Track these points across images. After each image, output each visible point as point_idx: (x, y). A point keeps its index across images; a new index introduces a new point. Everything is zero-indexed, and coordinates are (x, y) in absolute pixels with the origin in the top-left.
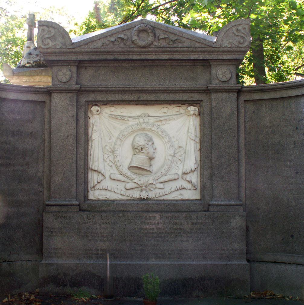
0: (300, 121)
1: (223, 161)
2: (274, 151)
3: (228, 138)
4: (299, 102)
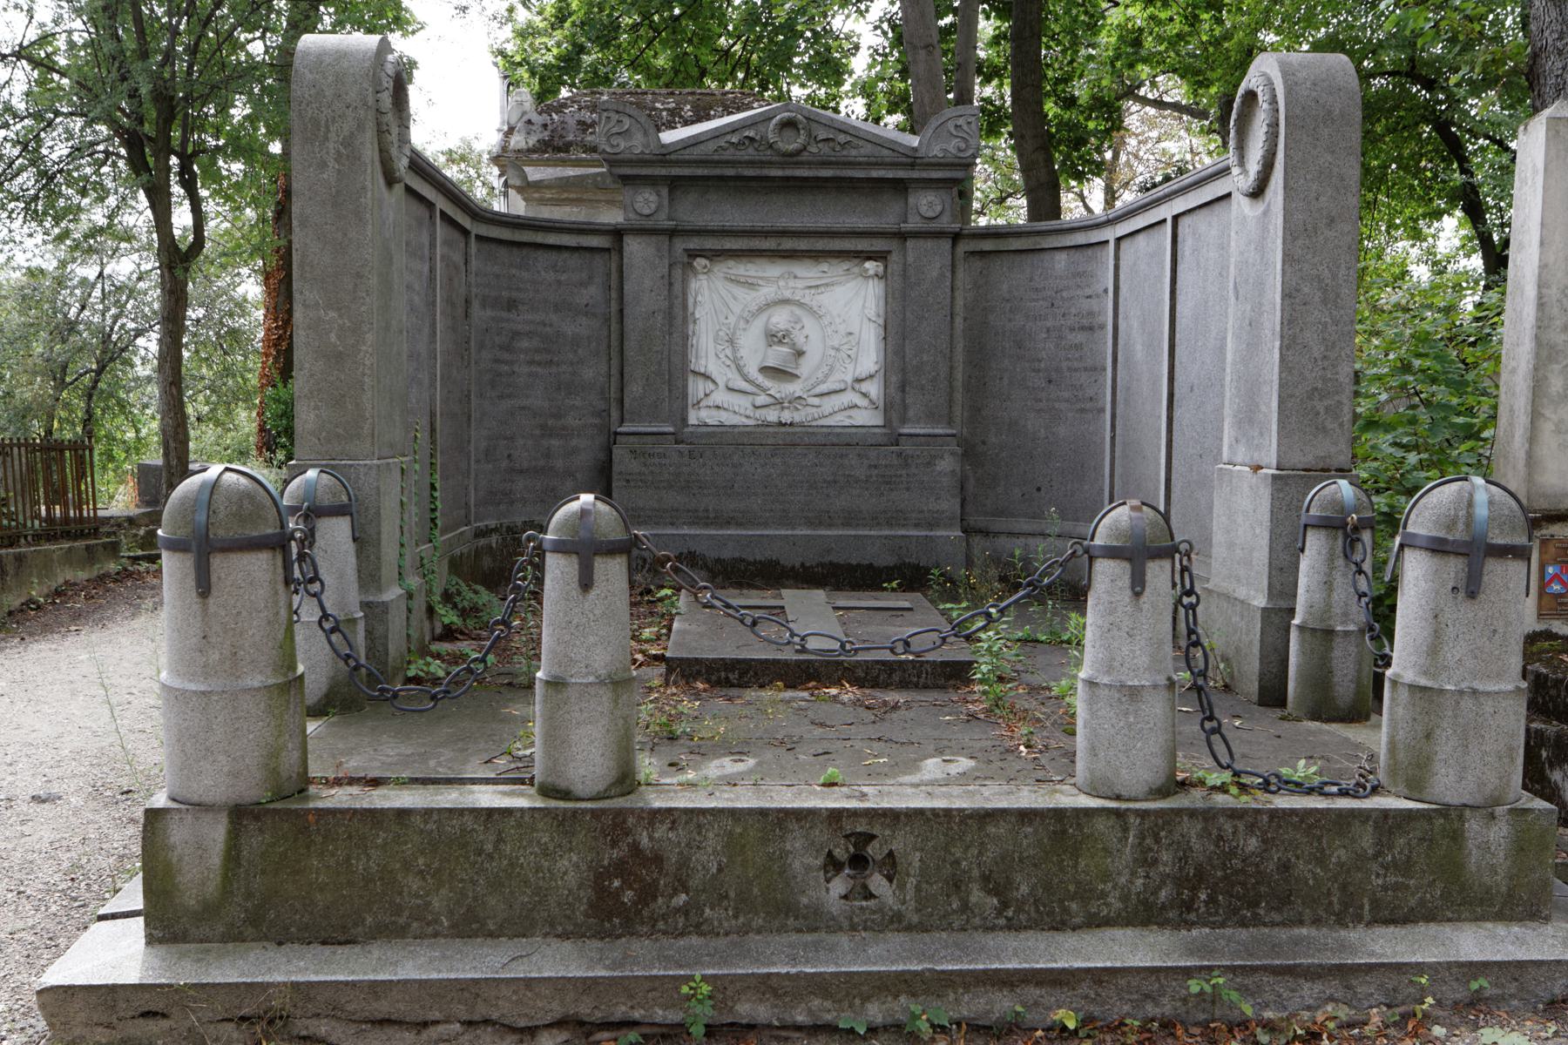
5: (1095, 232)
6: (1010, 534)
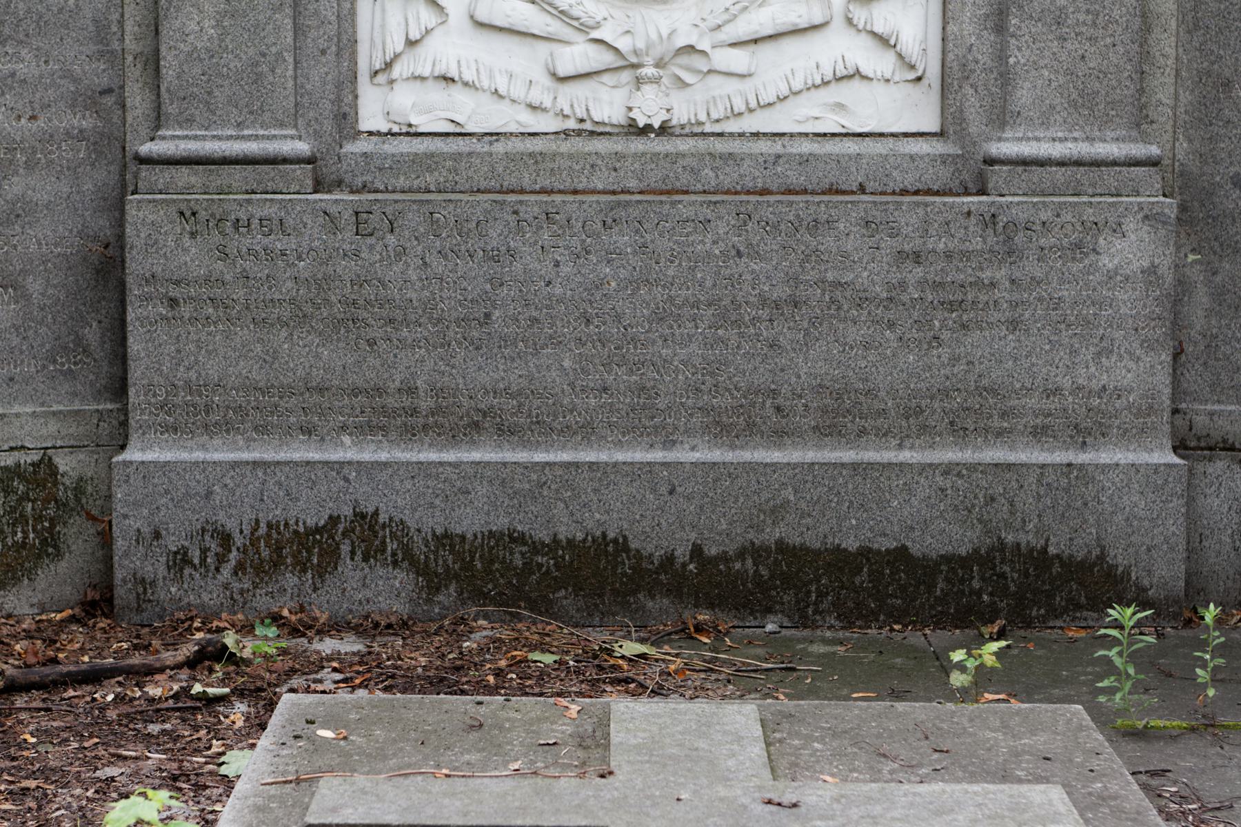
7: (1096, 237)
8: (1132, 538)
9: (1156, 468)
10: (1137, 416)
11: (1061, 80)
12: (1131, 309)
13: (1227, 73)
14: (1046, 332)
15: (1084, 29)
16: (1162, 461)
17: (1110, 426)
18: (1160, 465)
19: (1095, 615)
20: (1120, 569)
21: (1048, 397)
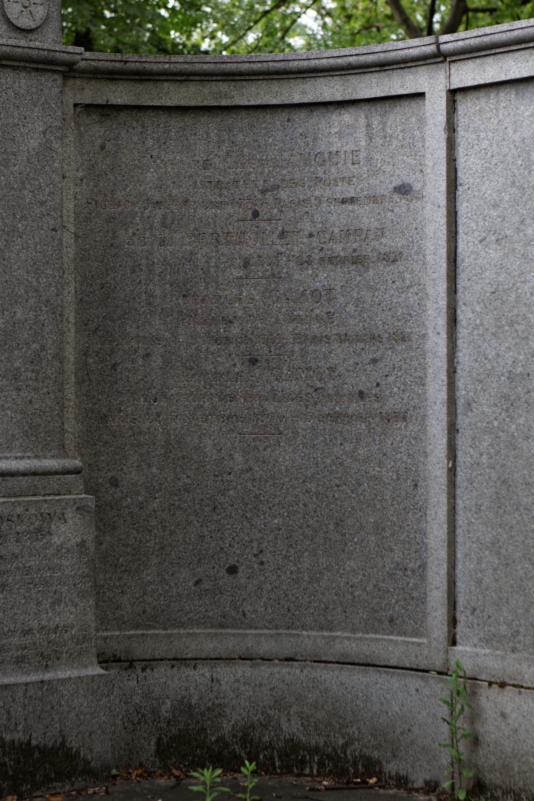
0: (267, 190)
1: (18, 315)
2: (171, 285)
3: (33, 236)
4: (266, 128)
5: (275, 86)
6: (178, 661)
7: (49, 523)
8: (80, 728)
9: (92, 678)
10: (77, 643)
11: (19, 417)
12: (71, 571)
13: (104, 410)
14: (22, 591)
15: (31, 383)
16: (95, 673)
17: (62, 652)
18: (95, 676)
19: (60, 784)
20: (74, 750)
21: (24, 636)
